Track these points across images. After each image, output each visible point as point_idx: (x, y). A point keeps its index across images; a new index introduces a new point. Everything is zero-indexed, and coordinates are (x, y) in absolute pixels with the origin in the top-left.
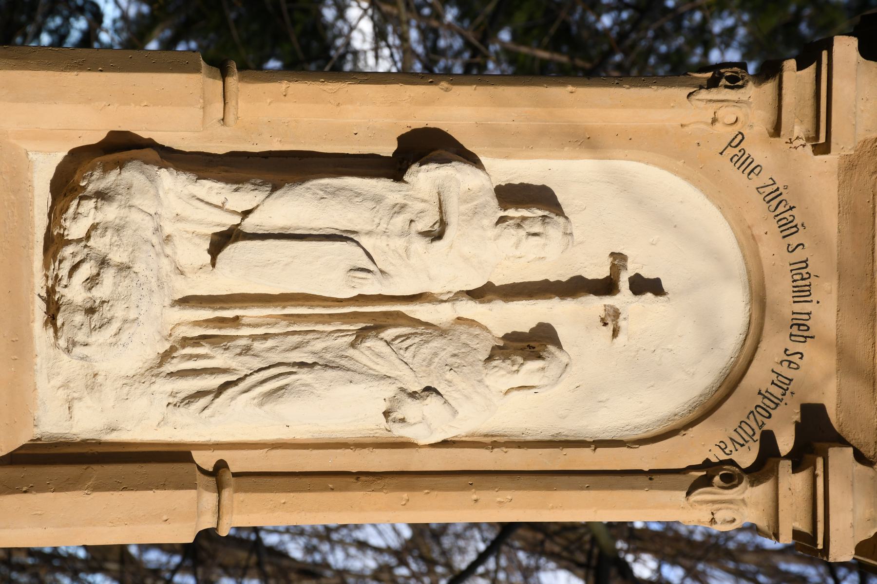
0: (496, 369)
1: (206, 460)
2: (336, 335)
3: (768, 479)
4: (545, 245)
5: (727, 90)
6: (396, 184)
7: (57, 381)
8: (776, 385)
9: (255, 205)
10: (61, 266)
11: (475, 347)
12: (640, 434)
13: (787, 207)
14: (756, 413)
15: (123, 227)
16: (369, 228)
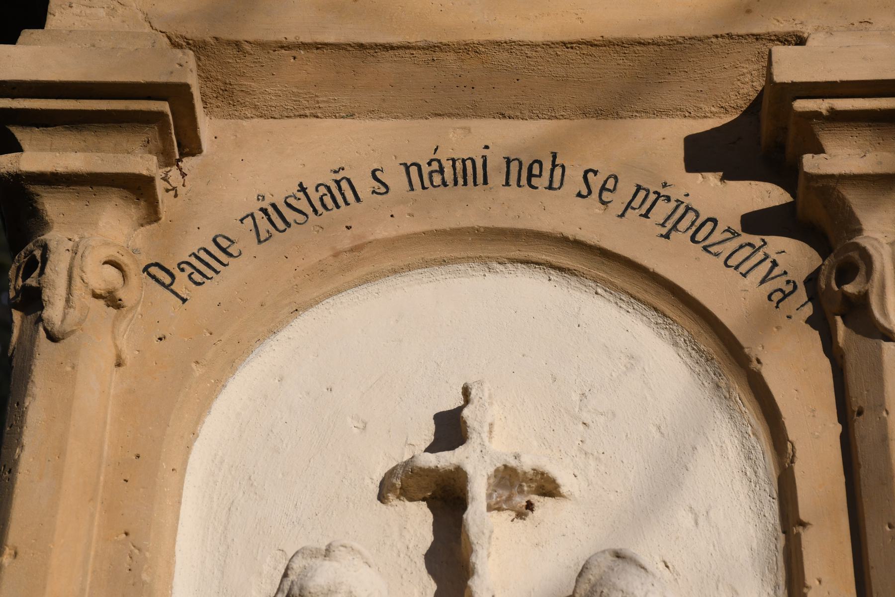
3: (844, 200)
5: (48, 270)
12: (762, 446)
13: (301, 195)
14: (707, 243)
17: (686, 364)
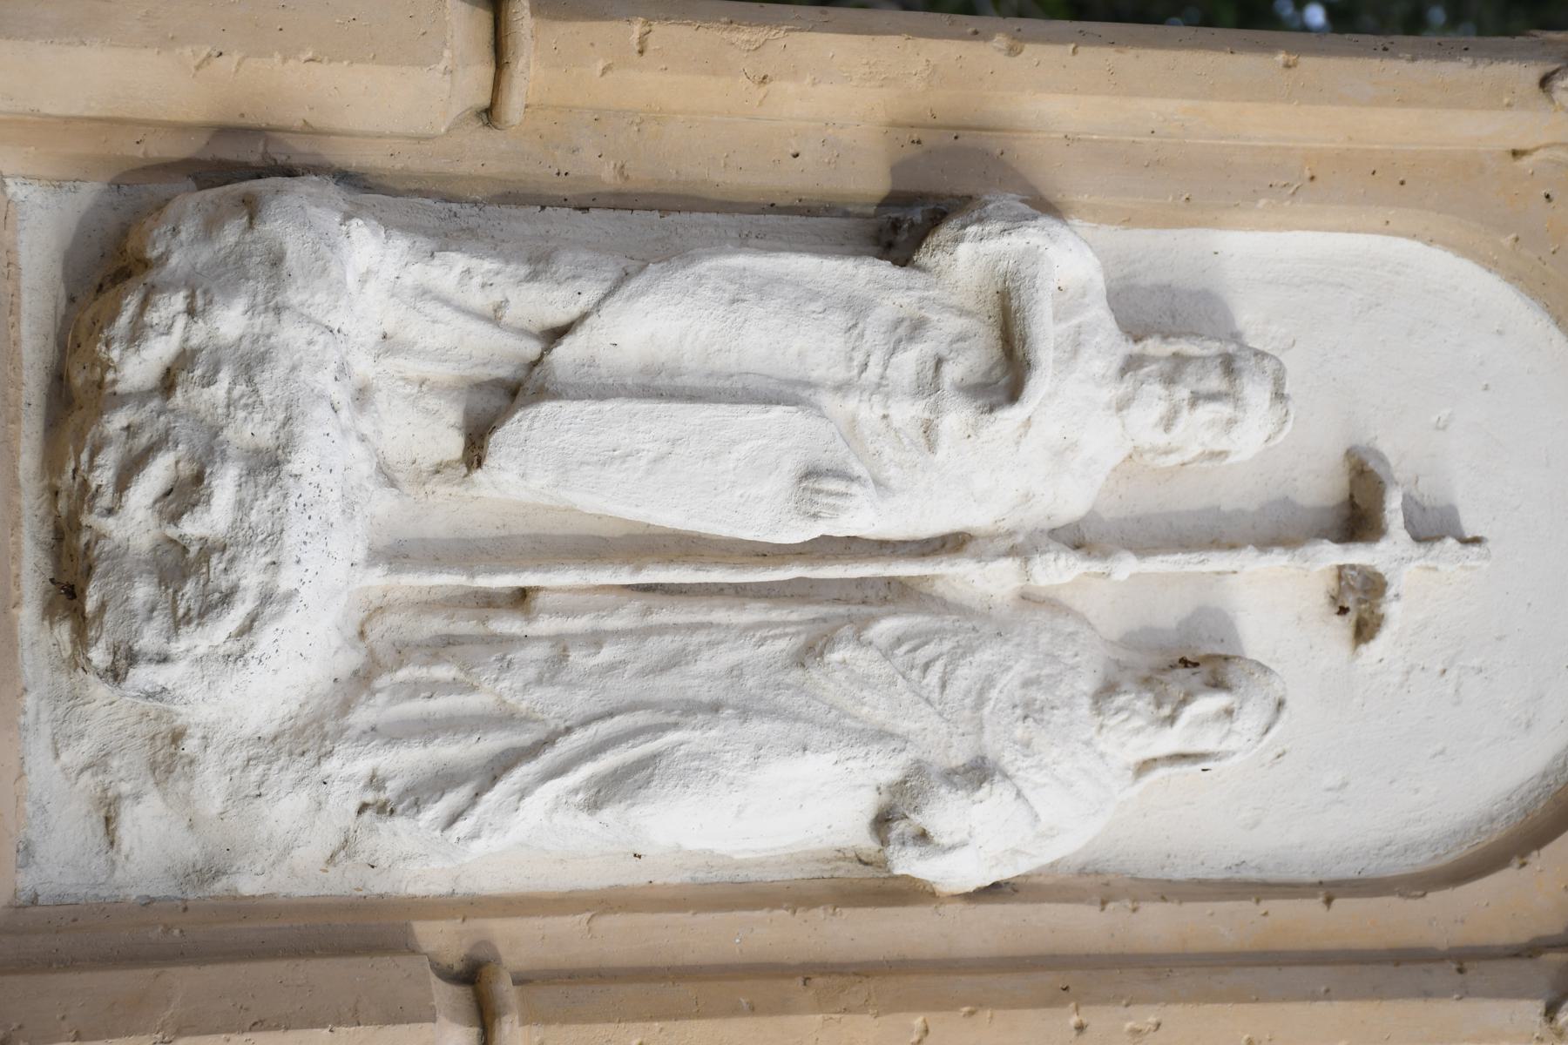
1: (444, 940)
4: (1231, 422)
6: (898, 272)
7: (76, 755)
10: (99, 460)
11: (1071, 662)
12: (1422, 861)
15: (263, 358)
16: (840, 374)
17: (1521, 786)
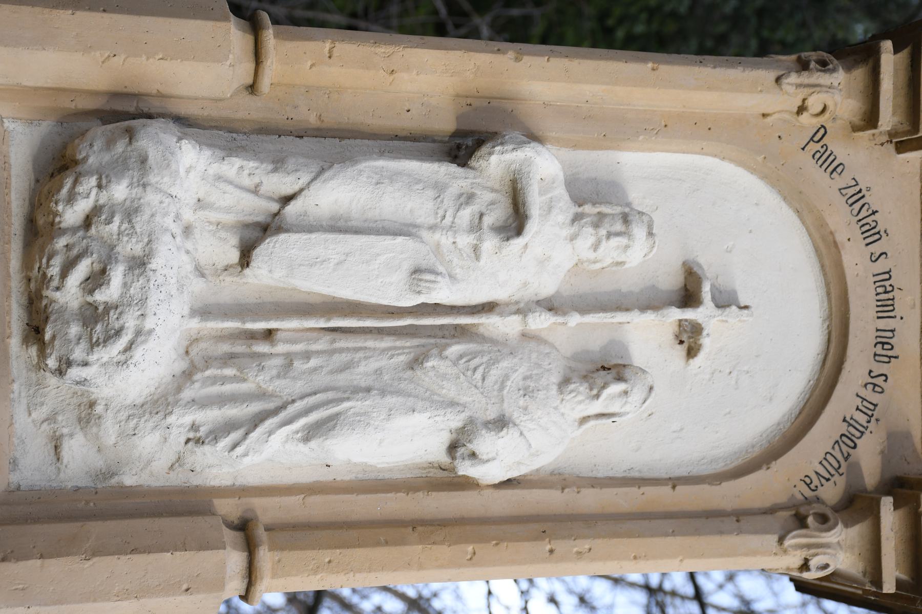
0: (573, 395)
1: (228, 508)
2: (393, 352)
4: (627, 247)
7: (40, 414)
8: (861, 411)
9: (296, 188)
12: (719, 467)
13: (870, 212)
14: (841, 443)
15: (137, 210)
16: (431, 221)
